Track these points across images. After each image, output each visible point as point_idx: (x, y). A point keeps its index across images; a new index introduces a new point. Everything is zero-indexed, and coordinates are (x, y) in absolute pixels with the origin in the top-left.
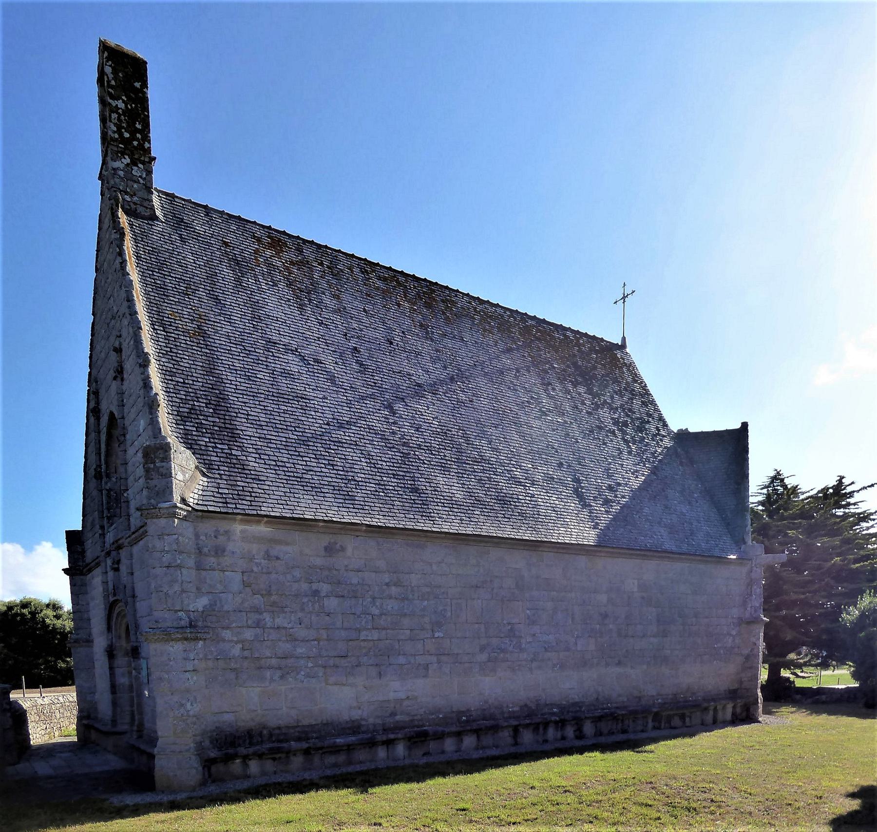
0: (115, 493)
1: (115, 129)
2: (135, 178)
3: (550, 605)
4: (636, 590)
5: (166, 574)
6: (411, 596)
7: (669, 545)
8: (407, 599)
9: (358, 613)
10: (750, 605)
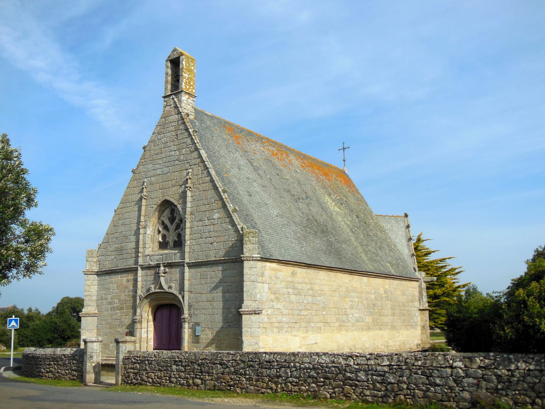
0: (151, 236)
4: (383, 293)
5: (252, 285)
7: (393, 272)
9: (301, 302)
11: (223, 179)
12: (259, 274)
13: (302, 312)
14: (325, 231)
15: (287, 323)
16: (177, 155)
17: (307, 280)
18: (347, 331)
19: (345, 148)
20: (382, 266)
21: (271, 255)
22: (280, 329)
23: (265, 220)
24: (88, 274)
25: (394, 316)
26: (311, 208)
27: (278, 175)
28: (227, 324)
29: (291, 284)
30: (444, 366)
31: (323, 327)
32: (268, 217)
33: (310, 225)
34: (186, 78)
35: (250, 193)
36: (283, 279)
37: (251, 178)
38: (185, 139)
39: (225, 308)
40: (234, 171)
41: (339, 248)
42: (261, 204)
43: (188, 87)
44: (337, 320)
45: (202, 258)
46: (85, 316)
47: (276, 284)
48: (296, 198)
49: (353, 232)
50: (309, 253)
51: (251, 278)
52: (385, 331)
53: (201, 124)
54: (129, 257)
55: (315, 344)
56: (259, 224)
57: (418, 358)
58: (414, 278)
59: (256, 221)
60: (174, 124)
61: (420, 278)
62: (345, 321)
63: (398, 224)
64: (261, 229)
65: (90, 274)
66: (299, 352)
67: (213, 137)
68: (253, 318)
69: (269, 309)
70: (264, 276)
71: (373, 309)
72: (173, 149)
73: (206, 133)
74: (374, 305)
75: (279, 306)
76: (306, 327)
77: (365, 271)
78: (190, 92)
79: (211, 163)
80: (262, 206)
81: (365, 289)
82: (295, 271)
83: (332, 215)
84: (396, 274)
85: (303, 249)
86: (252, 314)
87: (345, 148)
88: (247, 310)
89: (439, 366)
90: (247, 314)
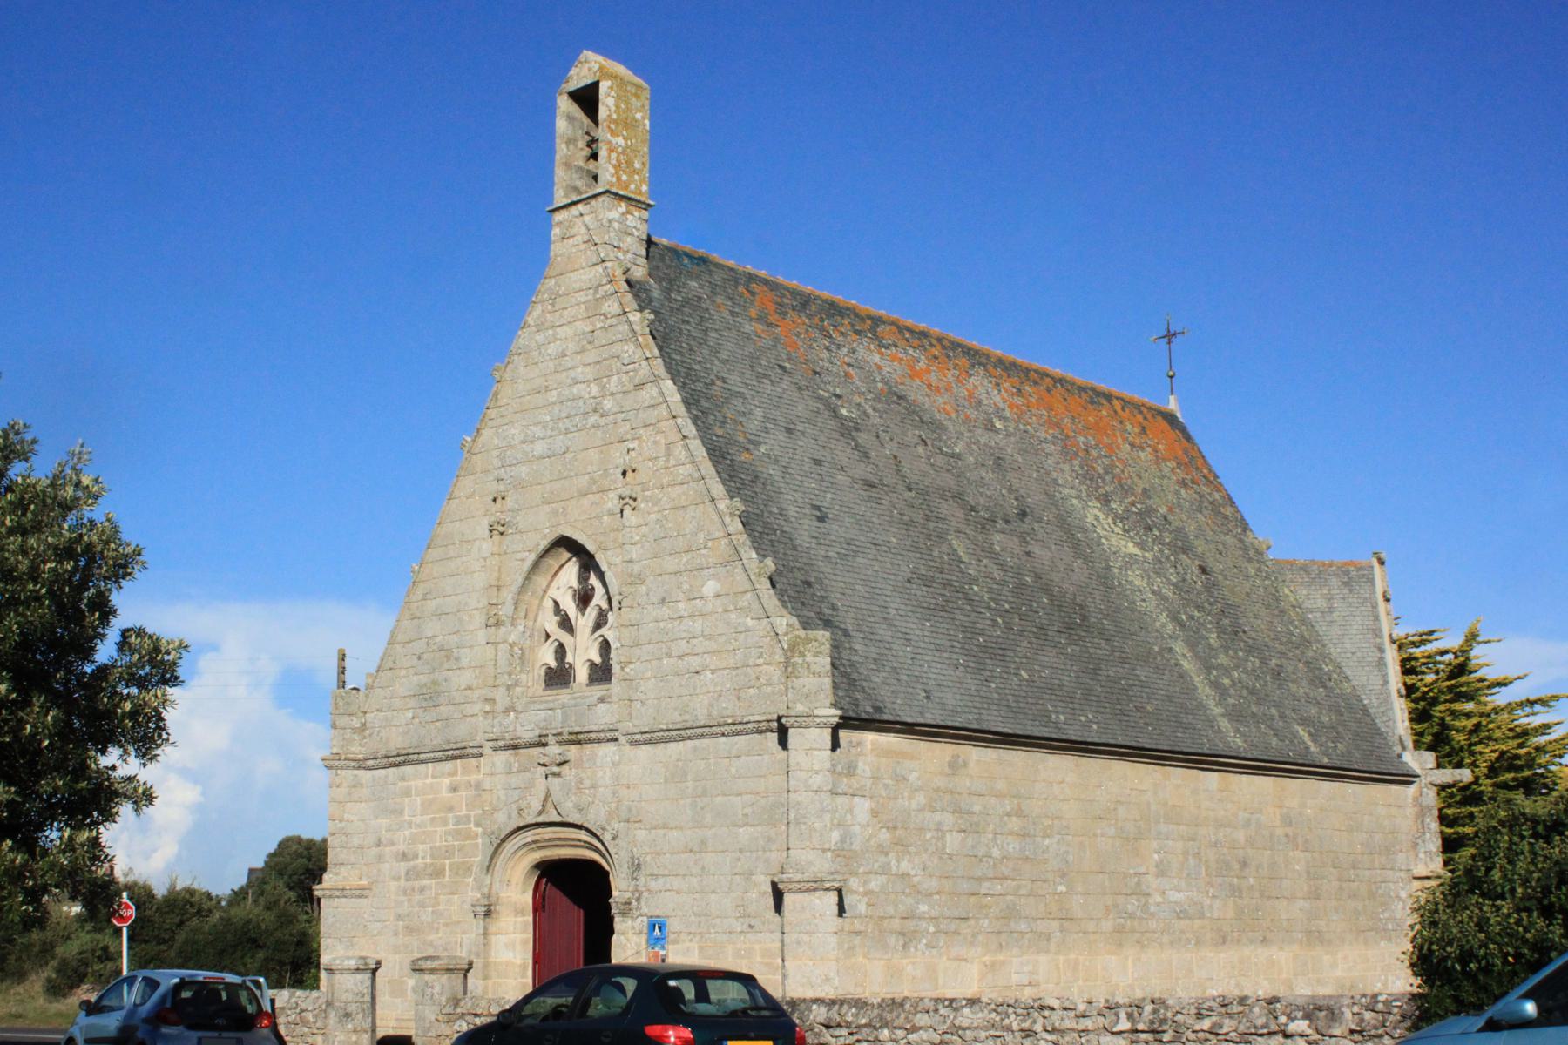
0: (521, 649)
1: (613, 171)
2: (629, 231)
3: (1179, 845)
4: (1278, 823)
6: (1032, 832)
8: (1029, 835)
9: (980, 854)
10: (1423, 850)
11: (734, 470)
12: (840, 766)
13: (986, 884)
14: (1076, 623)
15: (932, 918)
16: (592, 395)
17: (1001, 785)
18: (1143, 947)
19: (1172, 332)
20: (1276, 735)
21: (878, 709)
22: (908, 939)
23: (867, 595)
24: (337, 768)
25: (1319, 899)
26: (1036, 549)
27: (926, 445)
28: (742, 920)
29: (948, 797)
30: (1265, 1031)
31: (1058, 934)
32: (879, 585)
33: (1023, 604)
34: (620, 150)
35: (820, 511)
36: (920, 783)
37: (829, 459)
38: (618, 346)
39: (736, 871)
40: (773, 443)
41: (1120, 678)
42: (857, 543)
43: (624, 178)
44: (1107, 909)
45: (671, 718)
46: (330, 897)
47: (896, 798)
48: (981, 517)
49: (1182, 625)
50: (1010, 697)
51: (811, 781)
52: (1281, 949)
53: (668, 291)
54: (456, 716)
55: (1030, 984)
56: (845, 609)
57: (1204, 1012)
58: (1394, 772)
59: (835, 602)
60: (581, 297)
61: (1419, 772)
62: (1138, 913)
63: (1351, 591)
64: (850, 628)
65: (342, 768)
66: (905, 999)
67: (706, 331)
68: (817, 901)
69: (872, 876)
70: (854, 775)
71: (1238, 877)
72: (581, 378)
73: (684, 321)
74: (1244, 864)
75: (905, 866)
76: (999, 932)
77: (1208, 752)
78: (632, 192)
79: (695, 419)
80: (861, 550)
81: (1213, 810)
82: (962, 756)
83: (1108, 568)
84: (1325, 761)
85: (993, 685)
86: (815, 890)
87: (1174, 335)
88: (798, 877)
89: (1253, 1031)
90: (800, 890)
